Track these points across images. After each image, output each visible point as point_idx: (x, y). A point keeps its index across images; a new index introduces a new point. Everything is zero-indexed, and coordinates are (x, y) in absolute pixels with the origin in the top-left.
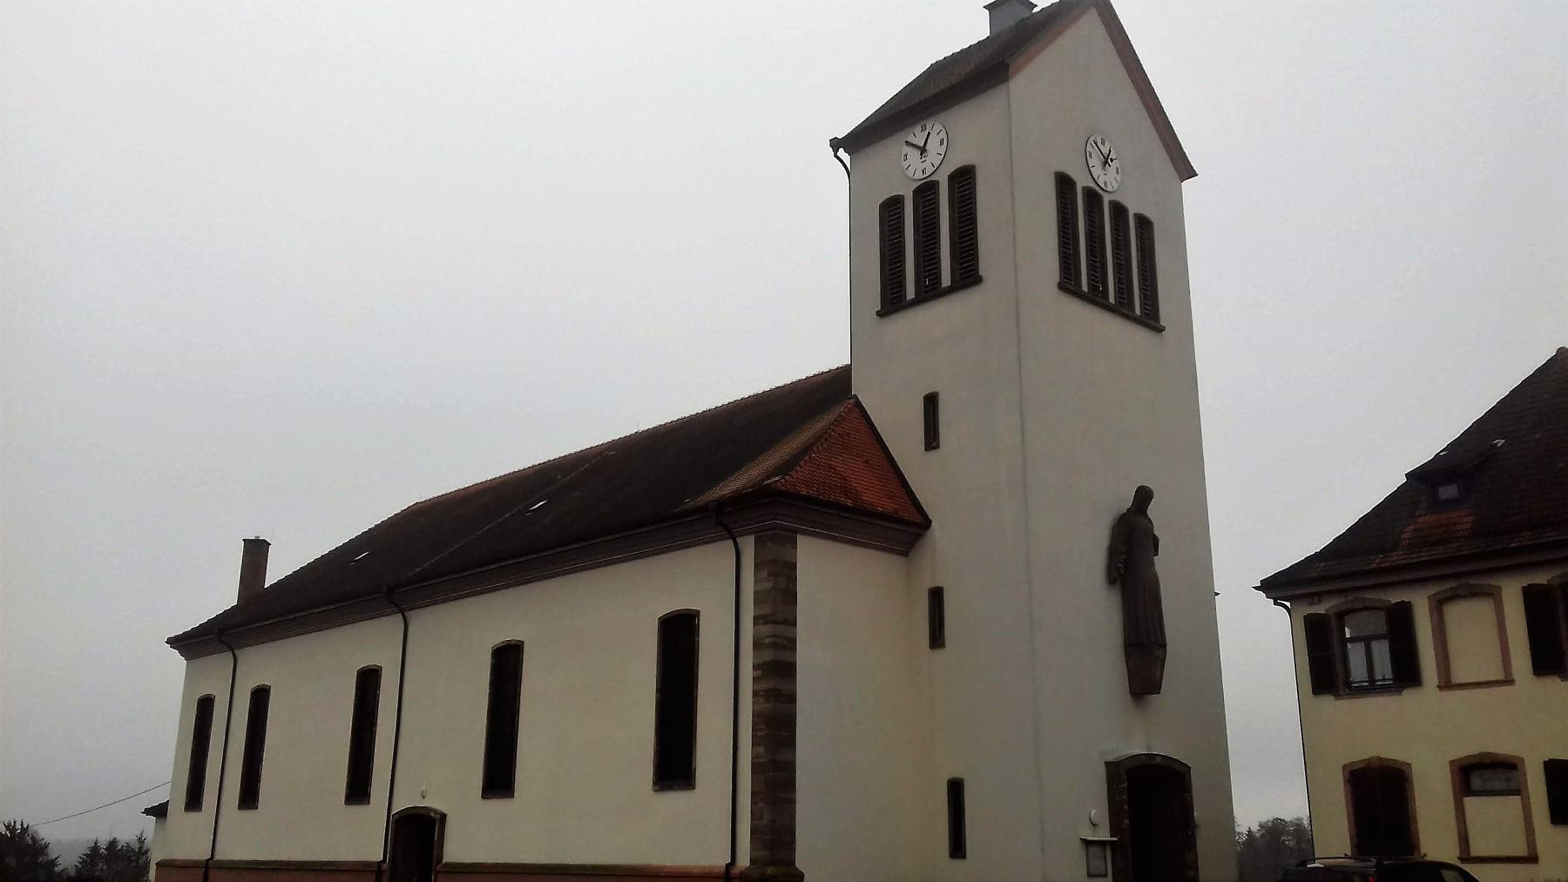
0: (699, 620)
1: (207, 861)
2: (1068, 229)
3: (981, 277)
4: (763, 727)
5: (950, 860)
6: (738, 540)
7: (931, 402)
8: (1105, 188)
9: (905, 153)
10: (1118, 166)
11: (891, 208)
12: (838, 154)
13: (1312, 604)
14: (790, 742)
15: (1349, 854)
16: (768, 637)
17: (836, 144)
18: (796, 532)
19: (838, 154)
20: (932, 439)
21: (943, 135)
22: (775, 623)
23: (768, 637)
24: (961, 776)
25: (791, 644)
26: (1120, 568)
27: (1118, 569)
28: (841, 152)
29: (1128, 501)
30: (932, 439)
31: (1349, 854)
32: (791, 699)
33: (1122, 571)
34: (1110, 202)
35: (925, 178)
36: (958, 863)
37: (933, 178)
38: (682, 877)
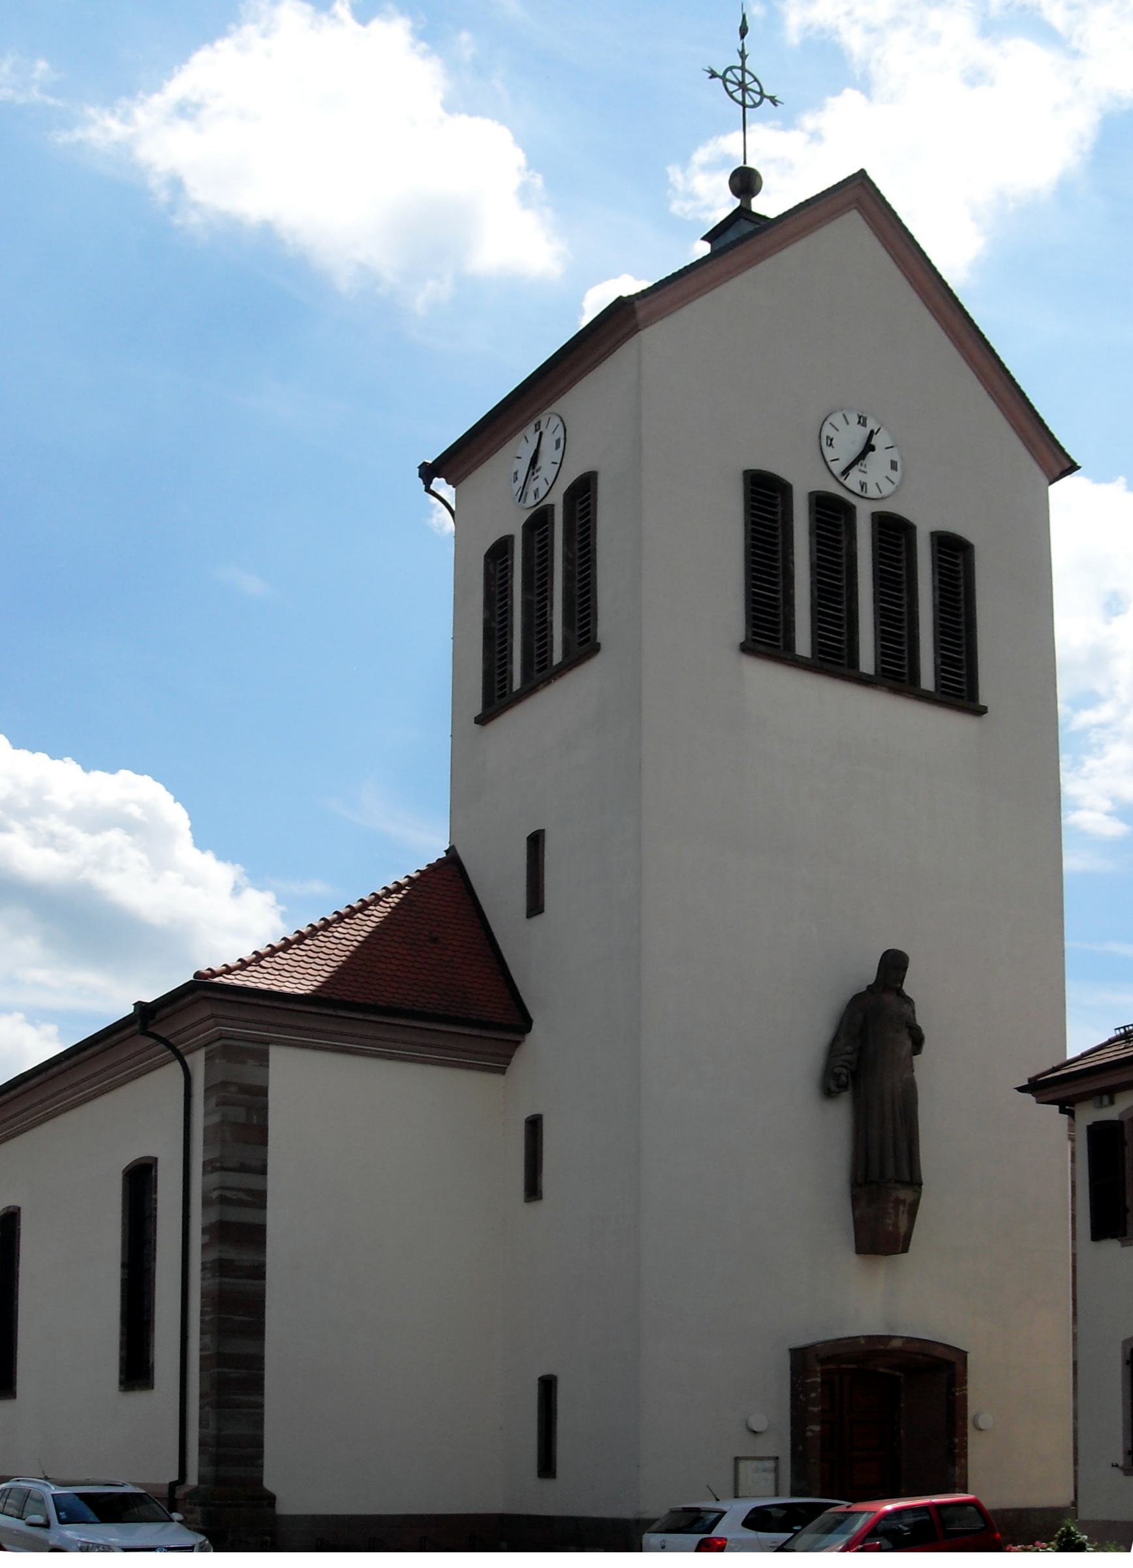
0: (156, 1171)
1: (173, 1486)
2: (775, 560)
3: (599, 644)
4: (209, 1309)
5: (539, 1480)
6: (187, 1059)
7: (536, 841)
8: (862, 494)
9: (515, 471)
10: (897, 459)
11: (499, 553)
12: (432, 487)
13: (1101, 1106)
14: (256, 1330)
15: (1121, 1463)
16: (215, 1189)
17: (428, 472)
18: (268, 1042)
19: (432, 487)
20: (535, 906)
21: (560, 433)
22: (223, 1169)
23: (215, 1189)
24: (555, 1374)
25: (259, 1199)
26: (840, 1074)
27: (837, 1076)
28: (438, 483)
29: (869, 973)
30: (535, 906)
31: (1121, 1463)
32: (258, 1272)
33: (844, 1078)
34: (934, 535)
35: (538, 504)
36: (547, 1484)
37: (547, 501)
38: (762, 1496)
